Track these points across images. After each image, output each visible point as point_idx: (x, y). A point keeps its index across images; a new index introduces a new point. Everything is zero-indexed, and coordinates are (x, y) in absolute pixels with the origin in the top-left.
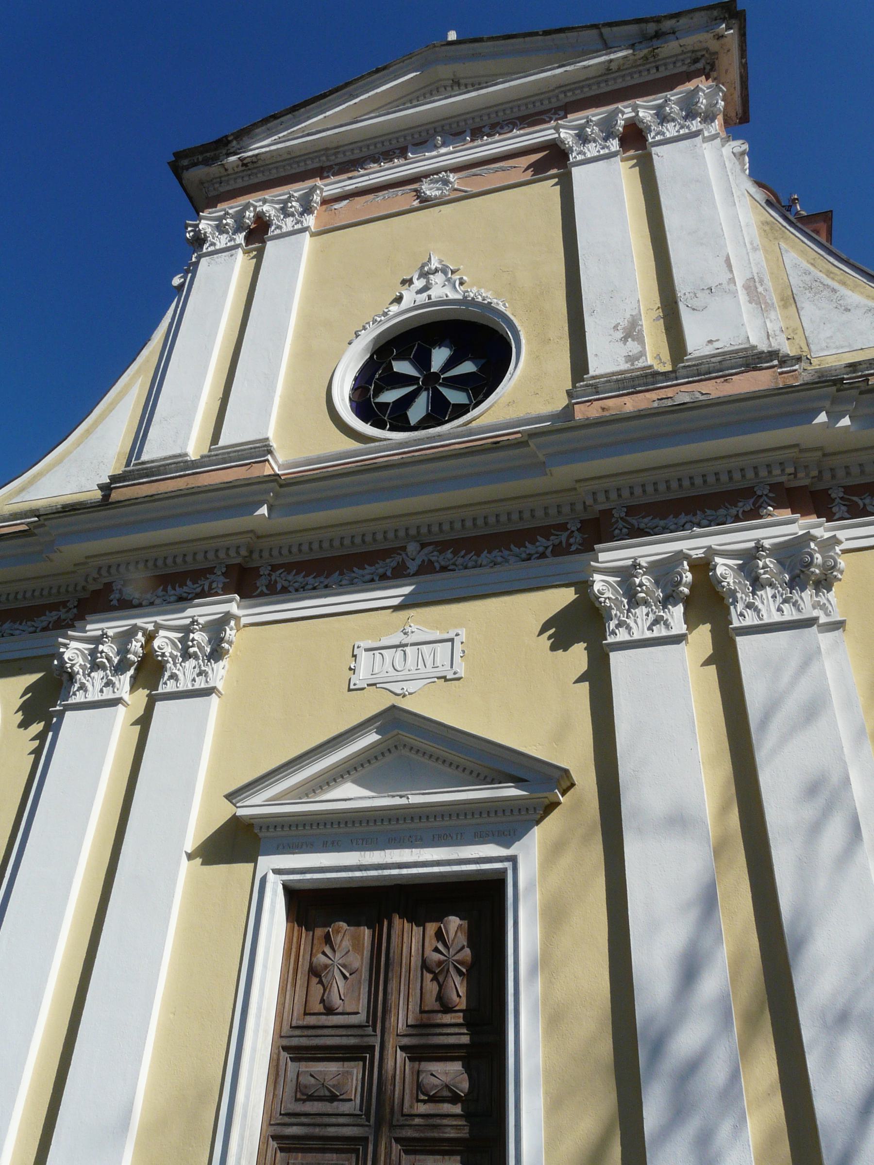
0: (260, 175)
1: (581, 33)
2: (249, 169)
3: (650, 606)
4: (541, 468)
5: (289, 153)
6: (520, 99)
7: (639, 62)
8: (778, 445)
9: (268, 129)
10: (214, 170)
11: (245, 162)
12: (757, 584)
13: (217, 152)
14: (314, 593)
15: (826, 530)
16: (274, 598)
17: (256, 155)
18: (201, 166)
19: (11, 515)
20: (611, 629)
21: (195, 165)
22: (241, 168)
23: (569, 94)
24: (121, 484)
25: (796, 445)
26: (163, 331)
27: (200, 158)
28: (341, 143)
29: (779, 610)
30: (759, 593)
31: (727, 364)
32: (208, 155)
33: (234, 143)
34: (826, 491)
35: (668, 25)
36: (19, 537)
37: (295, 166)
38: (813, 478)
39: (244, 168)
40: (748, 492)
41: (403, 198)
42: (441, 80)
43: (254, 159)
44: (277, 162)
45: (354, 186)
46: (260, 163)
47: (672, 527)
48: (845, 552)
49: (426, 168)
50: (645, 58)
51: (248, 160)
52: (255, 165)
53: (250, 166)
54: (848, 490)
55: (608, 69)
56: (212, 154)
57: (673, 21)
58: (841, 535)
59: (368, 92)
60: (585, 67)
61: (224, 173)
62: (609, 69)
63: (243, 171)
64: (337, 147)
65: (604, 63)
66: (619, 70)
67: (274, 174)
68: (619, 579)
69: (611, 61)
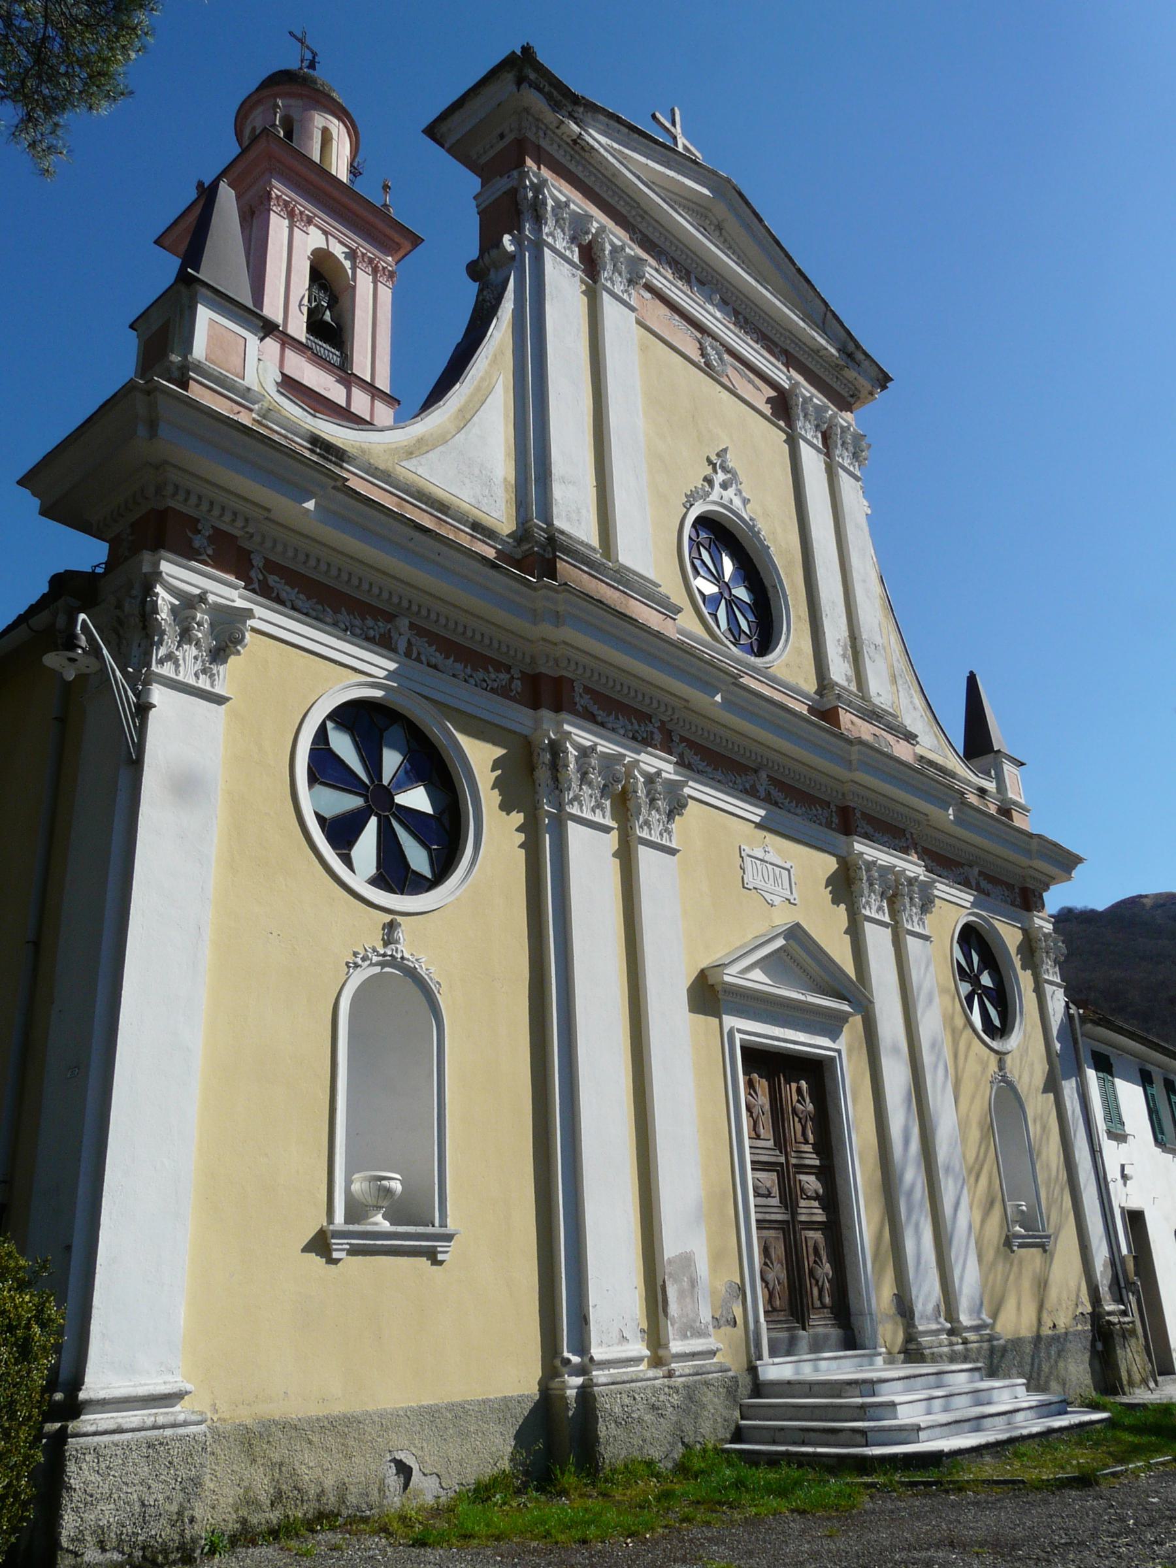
0: (580, 168)
1: (816, 299)
2: (573, 149)
3: (201, 651)
4: (849, 764)
5: (614, 175)
6: (766, 313)
7: (833, 364)
8: (591, 652)
9: (608, 125)
10: (550, 117)
11: (579, 141)
12: (185, 636)
13: (564, 102)
14: (718, 785)
15: (241, 597)
16: (752, 800)
17: (592, 148)
18: (541, 97)
19: (418, 492)
20: (160, 655)
21: (539, 89)
22: (569, 141)
23: (793, 345)
24: (565, 558)
25: (926, 815)
26: (506, 322)
27: (547, 89)
28: (650, 213)
29: (196, 675)
30: (185, 647)
31: (900, 729)
32: (555, 93)
33: (581, 109)
34: (250, 552)
35: (860, 356)
36: (238, 430)
37: (610, 193)
38: (247, 533)
39: (571, 143)
40: (645, 717)
41: (687, 341)
42: (710, 211)
43: (587, 148)
44: (599, 171)
45: (660, 285)
46: (587, 155)
47: (874, 838)
48: (254, 630)
49: (709, 324)
50: (837, 365)
51: (583, 143)
52: (581, 152)
53: (577, 148)
54: (267, 561)
55: (817, 351)
56: (560, 98)
57: (864, 357)
58: (259, 611)
59: (678, 173)
60: (814, 338)
61: (553, 126)
62: (818, 351)
63: (568, 144)
64: (645, 212)
65: (822, 345)
66: (821, 357)
67: (589, 181)
68: (177, 603)
69: (827, 349)
